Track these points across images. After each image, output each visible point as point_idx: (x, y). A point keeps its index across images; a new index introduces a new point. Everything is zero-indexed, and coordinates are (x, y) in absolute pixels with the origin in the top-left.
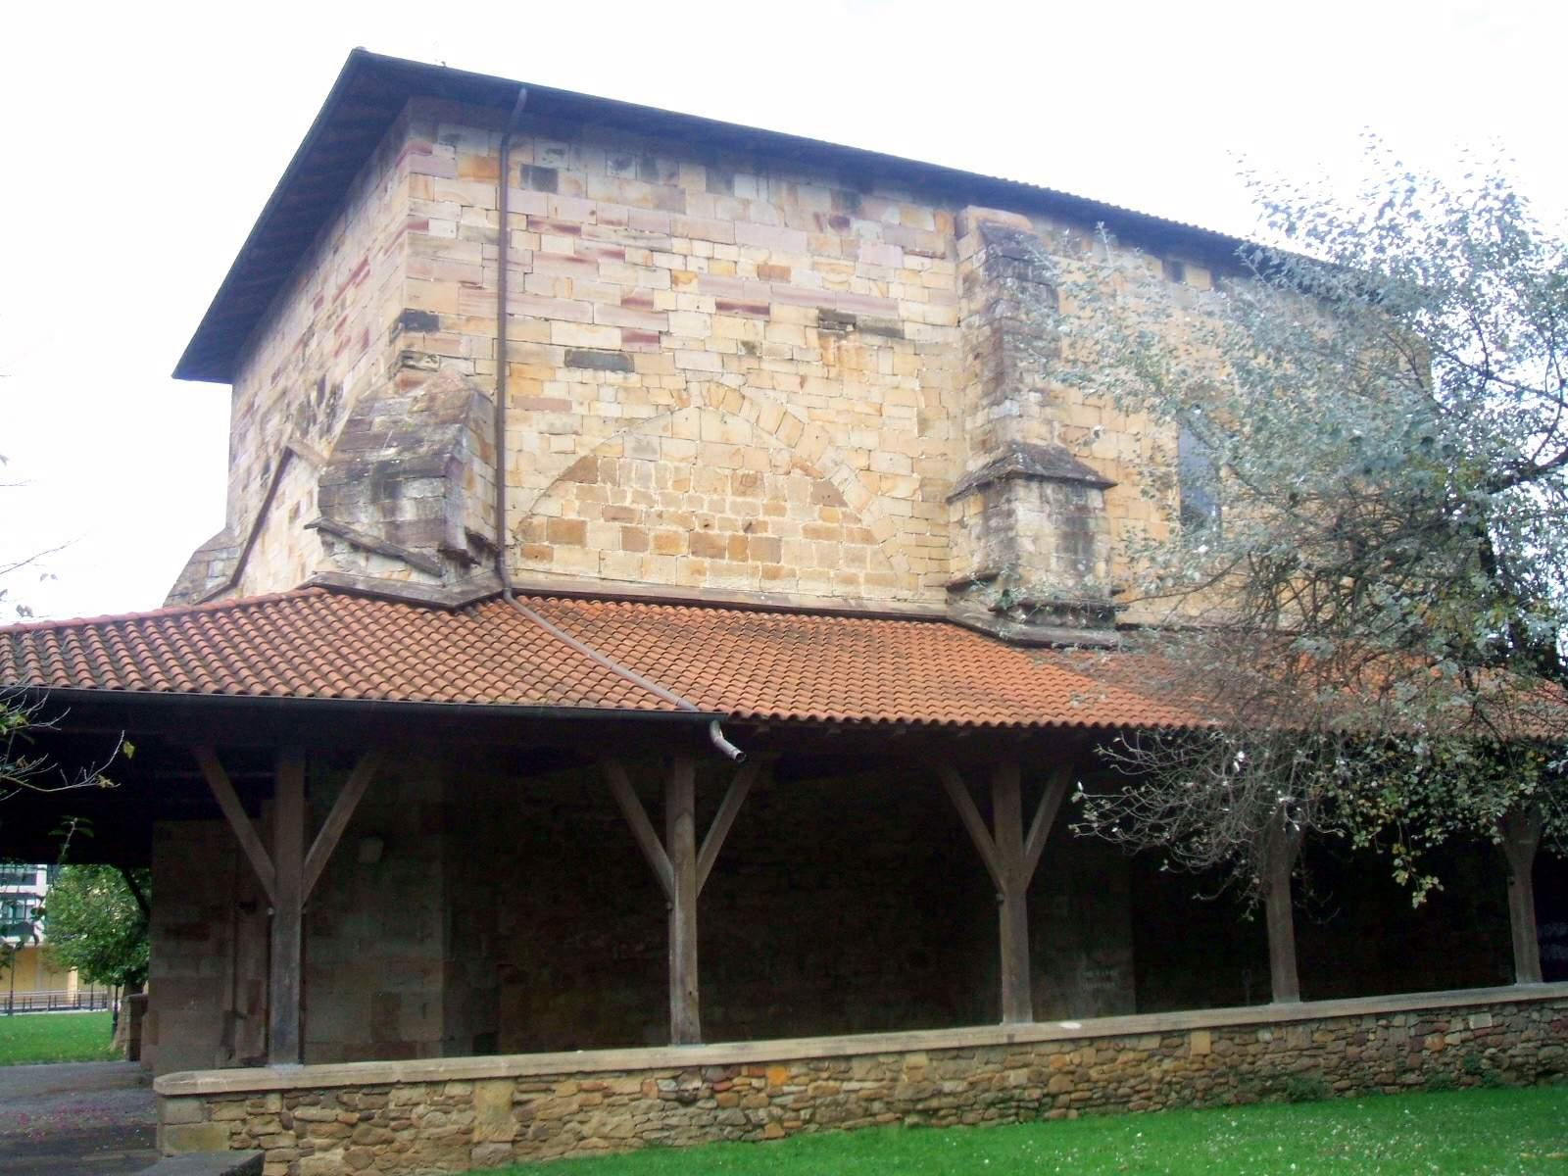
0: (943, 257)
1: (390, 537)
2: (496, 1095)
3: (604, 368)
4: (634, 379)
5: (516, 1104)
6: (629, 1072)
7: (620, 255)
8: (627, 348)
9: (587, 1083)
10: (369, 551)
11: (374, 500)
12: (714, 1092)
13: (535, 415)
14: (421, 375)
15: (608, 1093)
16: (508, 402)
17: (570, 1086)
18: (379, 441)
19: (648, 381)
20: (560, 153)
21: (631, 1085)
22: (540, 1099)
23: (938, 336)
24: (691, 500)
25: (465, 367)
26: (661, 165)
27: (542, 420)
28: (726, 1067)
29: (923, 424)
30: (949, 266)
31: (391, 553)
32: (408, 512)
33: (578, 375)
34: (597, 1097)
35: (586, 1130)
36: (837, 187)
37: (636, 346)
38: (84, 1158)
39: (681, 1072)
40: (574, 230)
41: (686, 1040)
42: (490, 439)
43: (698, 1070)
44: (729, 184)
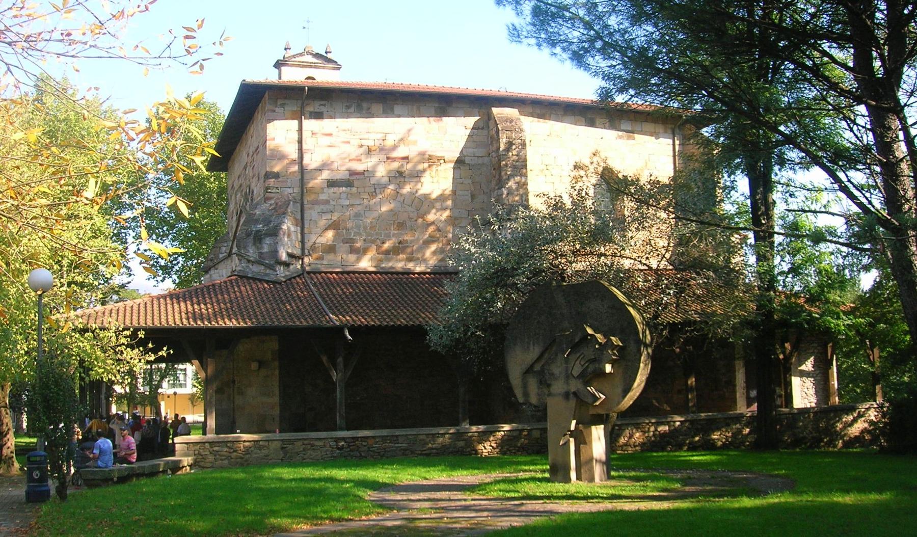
0: (483, 128)
1: (260, 257)
2: (277, 445)
3: (342, 186)
4: (354, 190)
5: (283, 448)
6: (320, 439)
7: (348, 142)
8: (351, 178)
9: (305, 442)
10: (253, 263)
11: (254, 244)
12: (349, 446)
13: (316, 207)
14: (273, 195)
15: (312, 445)
16: (305, 202)
17: (300, 443)
18: (257, 222)
19: (359, 190)
20: (324, 105)
21: (321, 443)
22: (290, 446)
23: (480, 161)
24: (377, 234)
25: (290, 191)
26: (365, 105)
27: (318, 208)
28: (353, 438)
29: (473, 197)
30: (485, 132)
31: (257, 263)
32: (266, 249)
33: (332, 190)
34: (309, 447)
35: (305, 457)
36: (437, 105)
37: (354, 177)
38: (268, 473)
39: (337, 440)
40: (330, 135)
41: (341, 429)
42: (299, 217)
43: (344, 439)
44: (392, 110)
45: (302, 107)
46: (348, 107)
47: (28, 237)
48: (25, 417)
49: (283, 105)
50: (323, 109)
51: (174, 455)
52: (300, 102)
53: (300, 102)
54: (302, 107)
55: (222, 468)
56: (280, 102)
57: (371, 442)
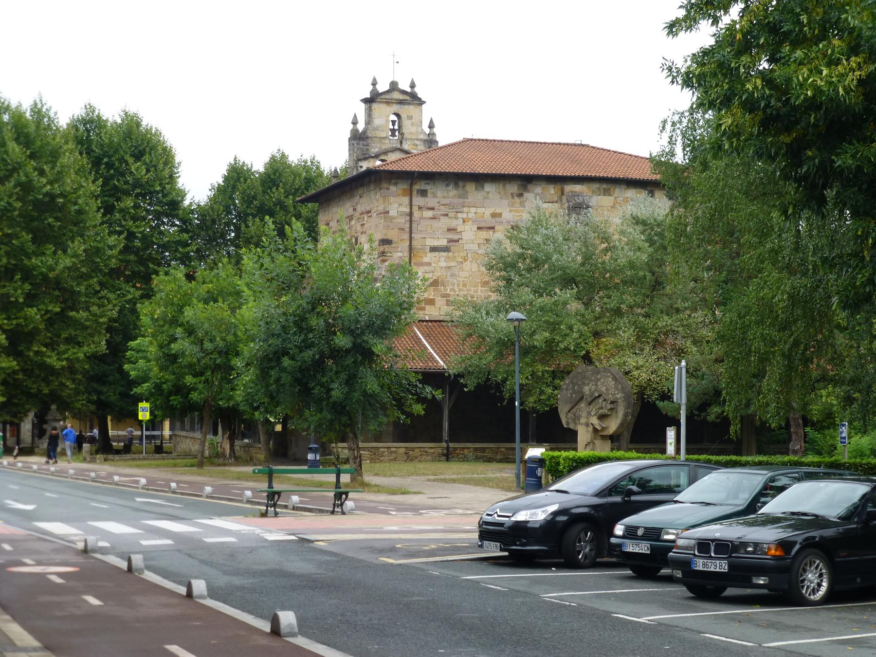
4: (451, 254)
7: (447, 215)
15: (426, 452)
22: (411, 453)
25: (400, 254)
26: (461, 184)
33: (433, 254)
45: (411, 186)
46: (447, 185)
47: (124, 223)
48: (855, 526)
49: (396, 184)
50: (428, 187)
51: (522, 441)
52: (409, 182)
53: (409, 182)
54: (411, 186)
55: (514, 349)
56: (393, 181)
57: (466, 451)
